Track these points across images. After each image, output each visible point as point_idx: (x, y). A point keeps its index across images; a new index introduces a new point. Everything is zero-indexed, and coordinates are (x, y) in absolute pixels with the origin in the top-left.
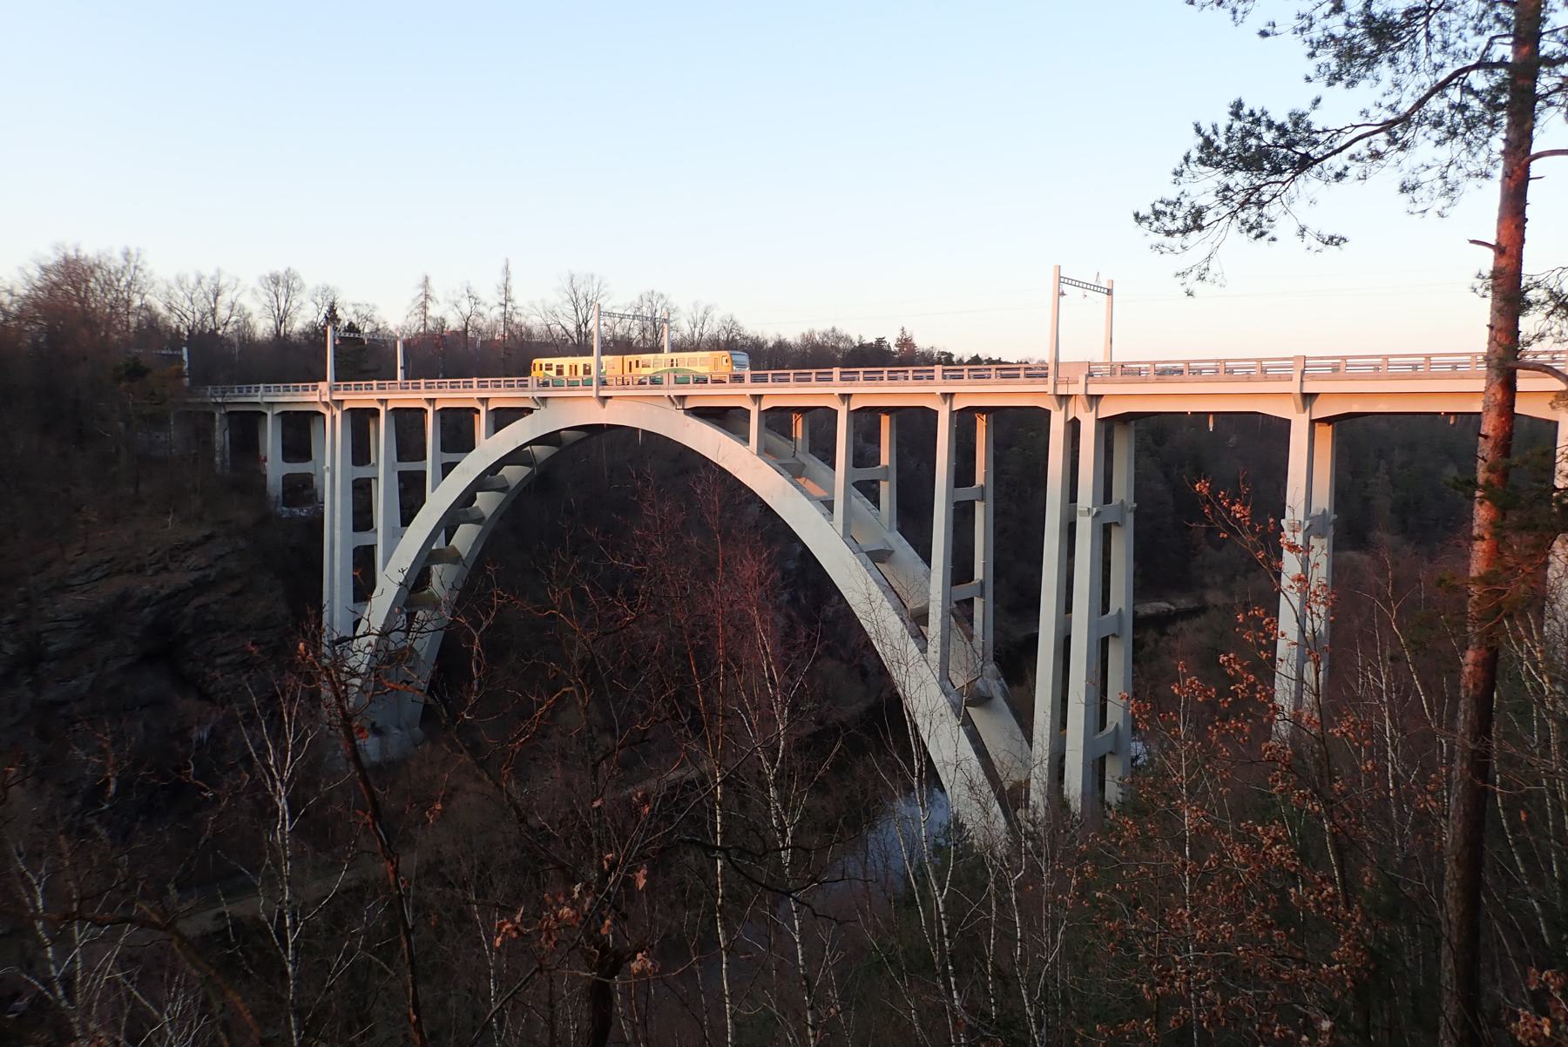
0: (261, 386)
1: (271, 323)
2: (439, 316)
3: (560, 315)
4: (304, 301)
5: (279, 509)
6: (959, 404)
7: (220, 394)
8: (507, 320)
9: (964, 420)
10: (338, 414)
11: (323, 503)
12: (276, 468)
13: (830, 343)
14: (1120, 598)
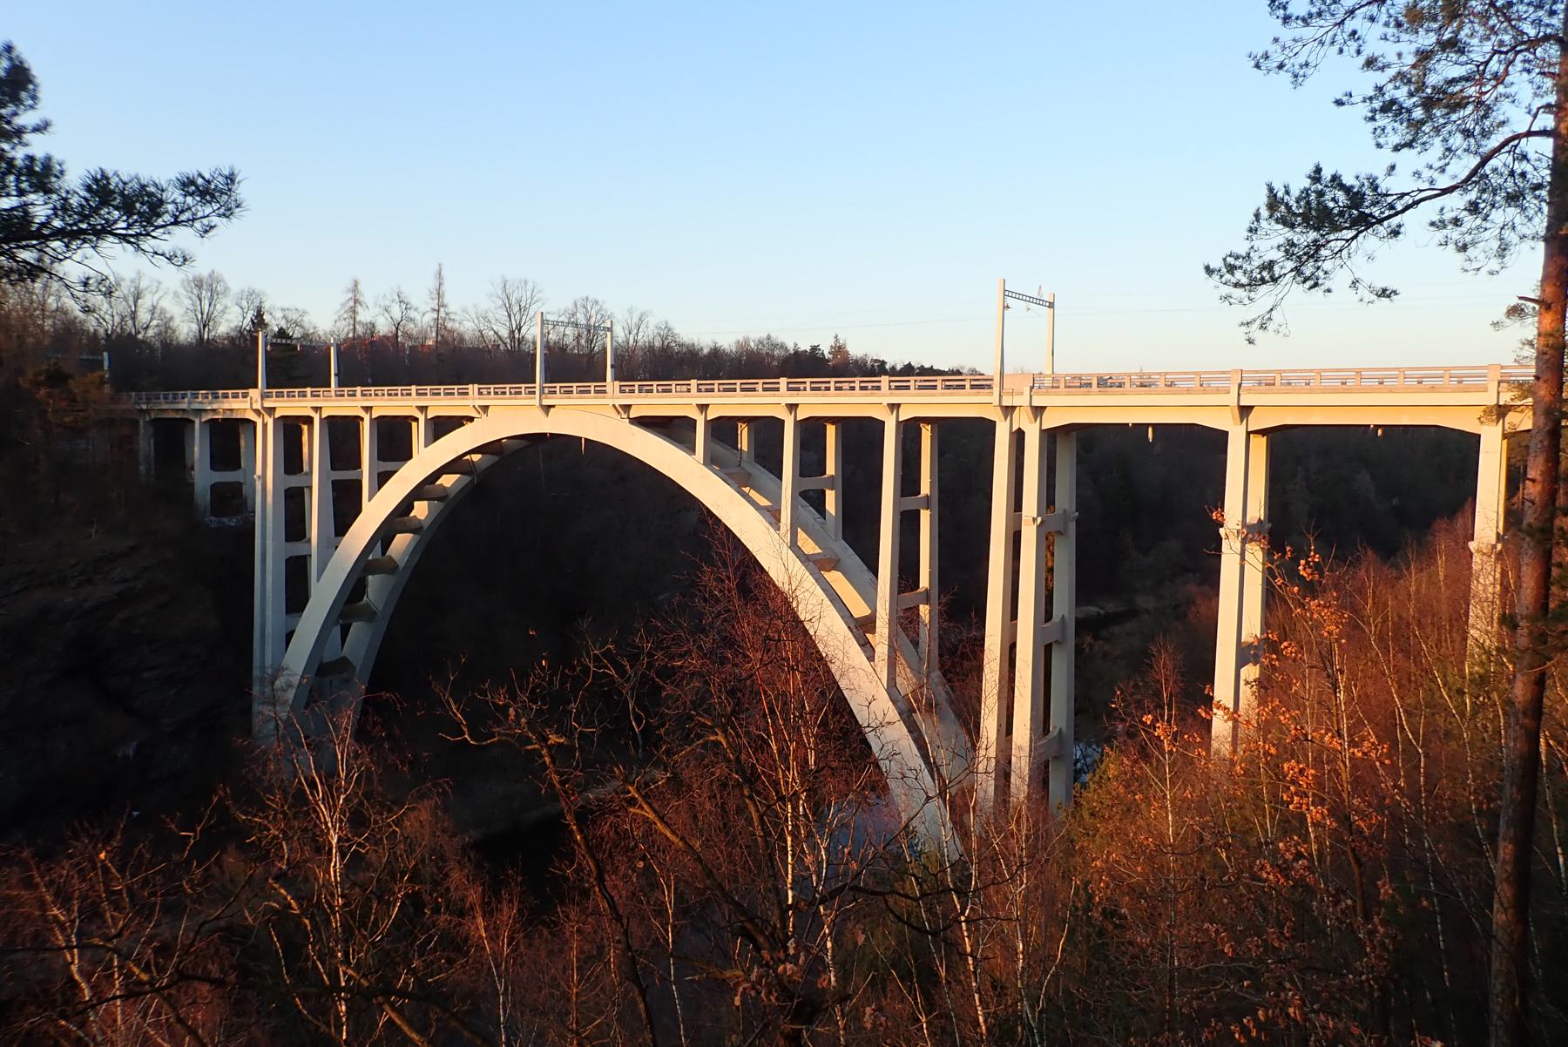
0: (189, 393)
1: (195, 327)
2: (369, 320)
3: (493, 321)
4: (229, 305)
5: (207, 519)
6: (905, 415)
7: (144, 400)
8: (439, 326)
9: (909, 430)
10: (270, 422)
11: (254, 512)
12: (203, 476)
13: (764, 351)
14: (1064, 606)
